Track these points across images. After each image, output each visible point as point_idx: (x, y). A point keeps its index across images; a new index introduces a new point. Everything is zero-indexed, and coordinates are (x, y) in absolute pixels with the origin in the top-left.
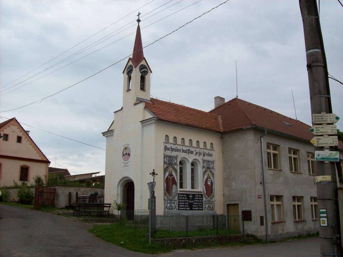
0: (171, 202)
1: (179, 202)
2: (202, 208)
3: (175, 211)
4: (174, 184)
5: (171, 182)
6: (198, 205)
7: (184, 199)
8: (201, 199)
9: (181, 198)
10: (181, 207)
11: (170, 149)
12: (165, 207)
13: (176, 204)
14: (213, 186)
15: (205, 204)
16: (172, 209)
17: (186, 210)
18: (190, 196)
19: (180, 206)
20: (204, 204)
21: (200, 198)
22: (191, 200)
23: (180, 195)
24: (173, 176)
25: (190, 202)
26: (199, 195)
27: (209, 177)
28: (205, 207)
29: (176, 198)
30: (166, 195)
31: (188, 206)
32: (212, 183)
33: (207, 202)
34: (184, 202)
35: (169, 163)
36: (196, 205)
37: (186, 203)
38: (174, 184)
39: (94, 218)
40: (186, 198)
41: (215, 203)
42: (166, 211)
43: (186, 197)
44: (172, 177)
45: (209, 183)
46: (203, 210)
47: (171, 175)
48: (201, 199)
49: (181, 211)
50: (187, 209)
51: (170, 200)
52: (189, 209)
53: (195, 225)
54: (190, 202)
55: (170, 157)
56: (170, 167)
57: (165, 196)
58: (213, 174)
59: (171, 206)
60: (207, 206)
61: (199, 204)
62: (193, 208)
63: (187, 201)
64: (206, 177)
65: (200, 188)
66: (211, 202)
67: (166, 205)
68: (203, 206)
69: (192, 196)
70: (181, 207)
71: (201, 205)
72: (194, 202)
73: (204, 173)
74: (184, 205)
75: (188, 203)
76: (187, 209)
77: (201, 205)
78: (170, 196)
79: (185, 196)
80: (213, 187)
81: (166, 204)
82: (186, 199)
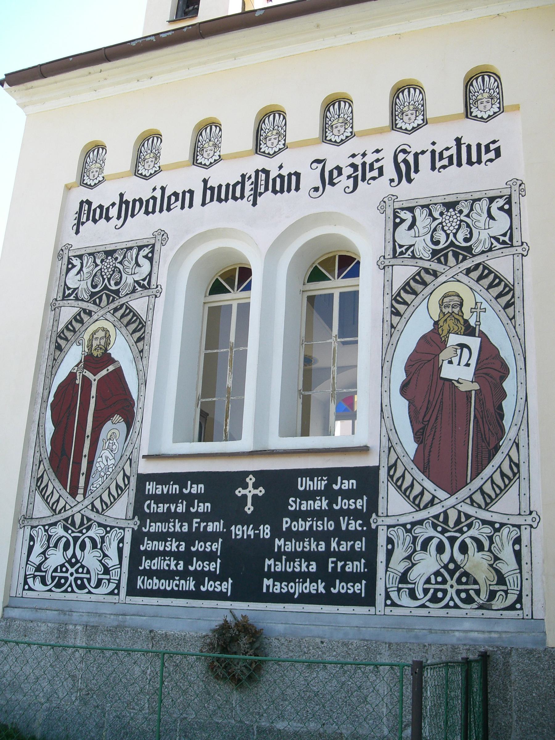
0: (76, 539)
1: (138, 538)
2: (359, 588)
3: (99, 602)
4: (117, 418)
5: (93, 402)
6: (321, 558)
7: (186, 517)
8: (361, 504)
9: (162, 508)
10: (150, 574)
11: (113, 212)
12: (31, 570)
13: (112, 552)
14: (509, 385)
15: (399, 553)
16: (82, 587)
17: (197, 595)
18: (240, 492)
19: (146, 564)
20: (389, 554)
21: (342, 504)
22: (245, 520)
23: (150, 487)
24: (111, 368)
25: (239, 531)
26: (331, 474)
27: (455, 319)
28: (404, 578)
29: (122, 509)
30: (42, 491)
31: (215, 566)
32: (492, 368)
33: (59, 531)
34: (179, 537)
35: (93, 295)
36: (292, 557)
37: (198, 546)
38: (117, 418)
39: (429, 693)
40: (204, 507)
41: (538, 543)
42: (30, 594)
43: (202, 498)
44: (104, 372)
45: (459, 371)
46: (380, 598)
47: (98, 360)
48: (361, 504)
49: (154, 601)
50: (208, 586)
51: (69, 524)
52: (226, 586)
53: (264, 723)
54: (239, 531)
55: (109, 253)
56: (95, 317)
57: (38, 498)
58: (506, 294)
59: (73, 562)
60: (427, 564)
61: (328, 553)
62: (267, 582)
63: (213, 527)
64: (419, 322)
65: (373, 423)
66: (95, 532)
67: (35, 559)
68: (372, 565)
69: (261, 491)
70: (150, 574)
71: (352, 556)
72: (277, 532)
73: (397, 299)
74: (177, 556)
75: (217, 547)
76: (208, 586)
77: (352, 556)
78: (73, 493)
79: (197, 489)
80: (503, 395)
81: (38, 549)
82: (197, 514)
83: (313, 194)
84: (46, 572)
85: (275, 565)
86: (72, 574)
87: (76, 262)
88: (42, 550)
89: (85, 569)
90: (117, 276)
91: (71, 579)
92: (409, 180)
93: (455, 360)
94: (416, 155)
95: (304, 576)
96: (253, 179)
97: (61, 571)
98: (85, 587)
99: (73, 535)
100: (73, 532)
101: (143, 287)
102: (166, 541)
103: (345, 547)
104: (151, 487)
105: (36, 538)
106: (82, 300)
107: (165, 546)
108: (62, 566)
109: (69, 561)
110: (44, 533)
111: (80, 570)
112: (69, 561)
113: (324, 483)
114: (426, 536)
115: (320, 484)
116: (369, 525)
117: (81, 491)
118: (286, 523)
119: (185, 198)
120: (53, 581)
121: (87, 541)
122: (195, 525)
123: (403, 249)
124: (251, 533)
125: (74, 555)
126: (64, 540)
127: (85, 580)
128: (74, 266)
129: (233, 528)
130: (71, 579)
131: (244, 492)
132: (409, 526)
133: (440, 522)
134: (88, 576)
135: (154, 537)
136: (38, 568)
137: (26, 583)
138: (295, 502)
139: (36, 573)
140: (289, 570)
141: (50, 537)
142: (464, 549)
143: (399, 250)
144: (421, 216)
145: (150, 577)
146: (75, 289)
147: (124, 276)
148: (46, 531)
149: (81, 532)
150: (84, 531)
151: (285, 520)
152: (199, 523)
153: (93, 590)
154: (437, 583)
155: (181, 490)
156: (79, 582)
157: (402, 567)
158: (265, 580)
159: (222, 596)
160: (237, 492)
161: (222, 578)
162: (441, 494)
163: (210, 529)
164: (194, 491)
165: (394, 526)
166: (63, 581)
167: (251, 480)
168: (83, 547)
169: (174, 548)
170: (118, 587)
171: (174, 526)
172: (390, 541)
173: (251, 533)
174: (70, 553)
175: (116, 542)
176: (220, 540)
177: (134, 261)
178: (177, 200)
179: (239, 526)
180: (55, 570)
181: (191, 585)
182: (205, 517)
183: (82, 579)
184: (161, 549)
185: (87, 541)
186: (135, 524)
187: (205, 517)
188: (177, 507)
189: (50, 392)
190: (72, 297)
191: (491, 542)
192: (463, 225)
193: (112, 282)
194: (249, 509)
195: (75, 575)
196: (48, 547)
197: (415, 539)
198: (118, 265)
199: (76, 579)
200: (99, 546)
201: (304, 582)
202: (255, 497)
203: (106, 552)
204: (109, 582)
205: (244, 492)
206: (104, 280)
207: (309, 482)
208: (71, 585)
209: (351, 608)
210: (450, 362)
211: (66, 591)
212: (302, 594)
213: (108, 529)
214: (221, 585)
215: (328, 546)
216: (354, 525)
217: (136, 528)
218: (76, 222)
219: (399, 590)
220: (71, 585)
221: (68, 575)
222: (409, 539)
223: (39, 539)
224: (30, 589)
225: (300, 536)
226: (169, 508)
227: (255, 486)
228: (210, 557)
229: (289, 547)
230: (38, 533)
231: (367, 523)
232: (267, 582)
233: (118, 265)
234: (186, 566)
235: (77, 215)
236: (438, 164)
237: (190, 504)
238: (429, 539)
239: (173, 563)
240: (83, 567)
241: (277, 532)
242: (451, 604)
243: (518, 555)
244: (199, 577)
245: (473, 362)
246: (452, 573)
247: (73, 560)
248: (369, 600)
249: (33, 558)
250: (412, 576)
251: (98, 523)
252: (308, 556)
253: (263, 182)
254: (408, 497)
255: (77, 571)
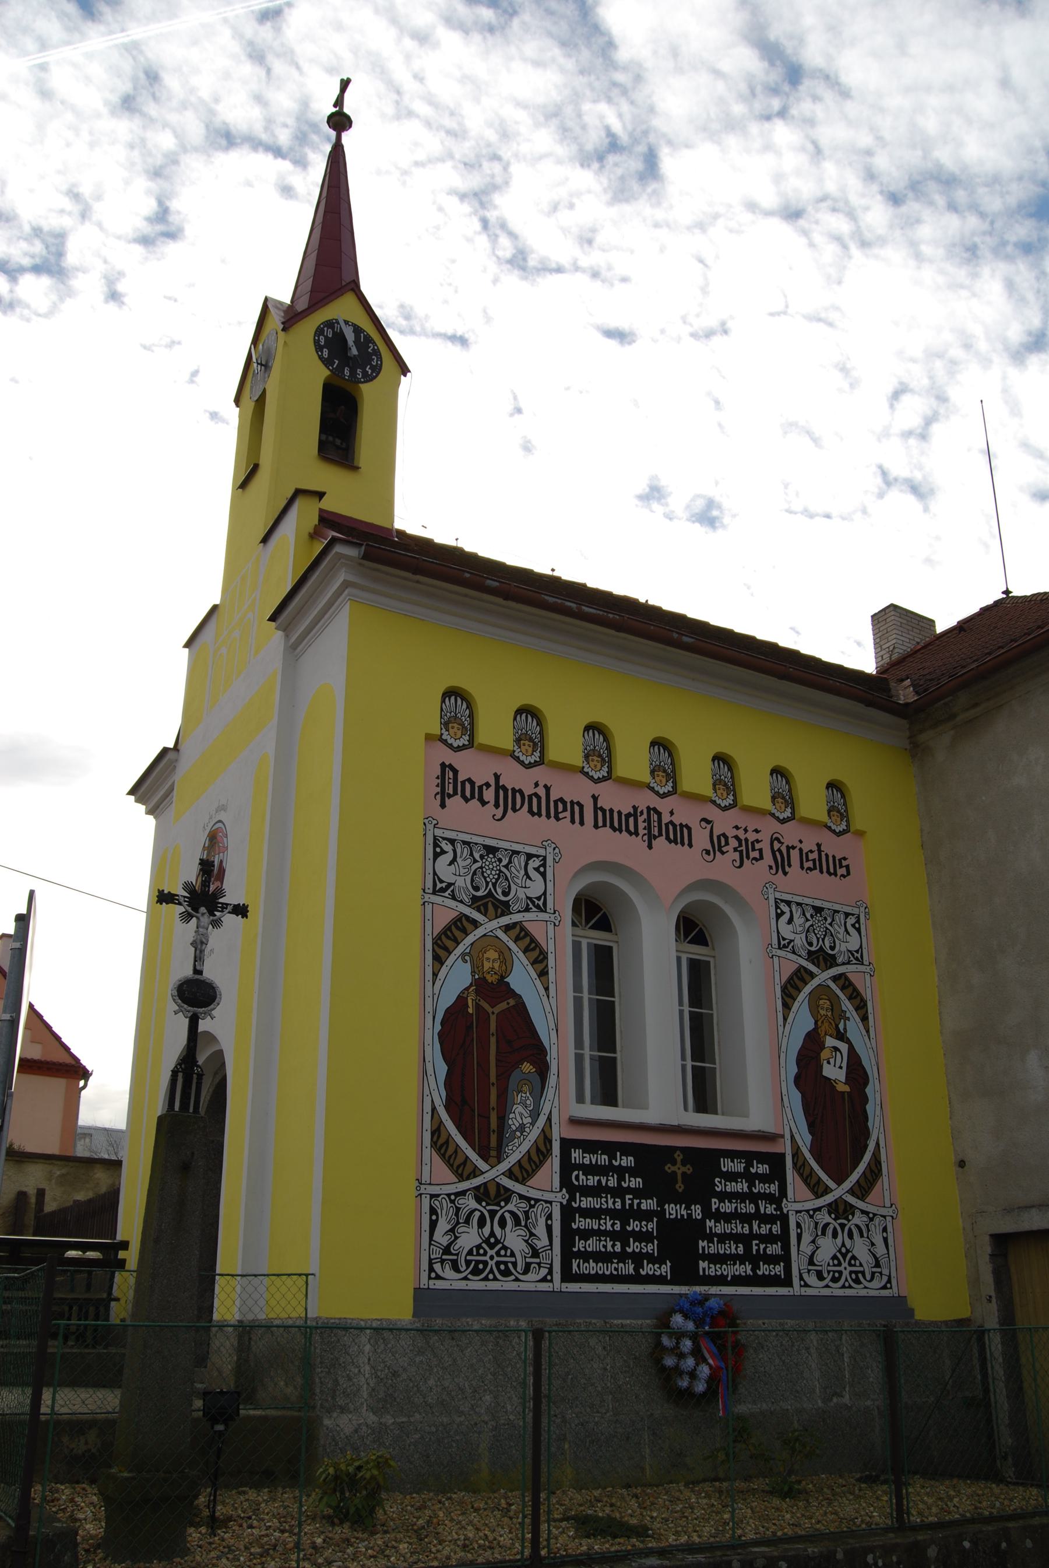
0: (493, 1214)
1: (568, 1213)
2: (779, 1269)
7: (618, 1192)
8: (774, 1188)
9: (592, 1181)
10: (586, 1256)
12: (437, 1253)
13: (541, 1230)
15: (806, 1238)
16: (506, 1273)
17: (637, 1279)
18: (669, 1168)
19: (580, 1245)
20: (799, 1237)
21: (759, 1188)
23: (576, 1155)
24: (512, 1002)
25: (673, 1211)
28: (811, 1262)
31: (652, 1248)
33: (824, 1218)
34: (613, 1214)
36: (723, 1238)
37: (634, 1226)
43: (633, 1172)
45: (834, 1071)
46: (796, 1280)
48: (774, 1188)
51: (481, 1194)
52: (666, 1269)
54: (673, 1211)
59: (491, 1241)
60: (827, 1248)
61: (752, 1236)
62: (703, 1265)
63: (648, 1204)
68: (786, 1247)
69: (688, 1169)
70: (586, 1256)
71: (770, 1238)
73: (437, 942)
74: (613, 1236)
75: (652, 1226)
76: (648, 1269)
77: (770, 1238)
79: (627, 1161)
81: (443, 1226)
82: (629, 1190)
83: (706, 856)
84: (457, 1255)
85: (709, 1247)
86: (492, 1258)
87: (447, 847)
88: (450, 1227)
89: (509, 1252)
90: (505, 884)
91: (492, 1263)
92: (785, 873)
93: (832, 1061)
94: (788, 848)
95: (734, 1258)
96: (645, 816)
97: (478, 1254)
98: (510, 1274)
99: (488, 1208)
100: (488, 1204)
101: (538, 907)
102: (600, 1219)
103: (764, 1230)
104: (577, 1155)
105: (439, 1211)
106: (461, 902)
107: (600, 1224)
108: (479, 1247)
109: (487, 1241)
110: (450, 1205)
111: (503, 1252)
112: (487, 1241)
113: (743, 1165)
114: (825, 1222)
115: (738, 1166)
116: (781, 1209)
117: (493, 1153)
118: (715, 1203)
119: (574, 810)
120: (468, 1267)
121: (507, 1215)
122: (628, 1202)
123: (444, 885)
124: (684, 1213)
125: (492, 1234)
126: (477, 1214)
127: (510, 1265)
128: (443, 852)
129: (666, 1206)
130: (492, 1263)
131: (673, 1168)
132: (811, 1213)
133: (481, 1194)
134: (513, 1259)
135: (586, 1213)
136: (447, 1250)
137: (431, 1269)
138: (720, 1182)
139: (444, 1257)
140: (722, 1252)
141: (458, 1209)
142: (503, 1224)
143: (782, 943)
144: (463, 852)
145: (586, 1261)
146: (450, 885)
147: (513, 887)
148: (811, 1217)
149: (498, 1204)
150: (503, 1204)
151: (713, 1200)
152: (632, 1200)
153: (521, 1277)
154: (834, 1265)
155: (610, 1161)
156: (502, 1267)
157: (445, 1241)
158: (701, 1262)
159: (660, 1280)
160: (666, 1168)
161: (660, 1261)
162: (482, 1165)
163: (643, 1207)
164: (624, 1163)
165: (800, 1212)
166: (481, 1266)
167: (678, 1156)
168: (503, 1224)
169: (609, 1228)
170: (550, 1272)
171: (607, 1202)
172: (798, 1225)
173: (684, 1213)
174: (487, 1231)
175: (544, 1219)
176: (655, 1219)
177: (522, 872)
178: (565, 810)
179: (672, 1205)
180: (470, 1252)
181: (629, 1268)
182: (637, 1193)
183: (505, 1263)
184: (596, 1227)
185: (507, 1215)
186: (562, 1197)
187: (637, 1193)
188: (608, 1180)
189: (434, 1018)
190: (446, 894)
191: (527, 1218)
192: (829, 934)
193: (499, 891)
194: (680, 1187)
195: (496, 1259)
196: (458, 1223)
197: (816, 1224)
198: (503, 869)
199: (498, 1264)
200: (523, 1223)
201: (735, 1264)
202: (684, 1174)
203: (533, 1231)
204: (540, 1267)
205: (673, 1168)
206: (487, 883)
207: (731, 1164)
208: (491, 1271)
209: (750, 1289)
210: (829, 1063)
211: (486, 1279)
212: (734, 1276)
213: (532, 1202)
214: (660, 1268)
215: (751, 1228)
216: (770, 1209)
217: (565, 1202)
218: (439, 789)
219: (809, 1271)
220: (491, 1271)
221: (487, 1258)
222: (812, 1225)
223: (444, 1212)
224: (438, 1277)
225: (728, 1218)
226: (599, 1181)
227: (684, 1164)
228: (643, 1237)
229: (719, 1228)
230: (441, 1203)
231: (779, 1208)
232: (703, 1265)
233: (503, 869)
234: (623, 1247)
235: (439, 781)
236: (806, 865)
237: (621, 1178)
238: (827, 1225)
239: (610, 1244)
240: (505, 1248)
241: (707, 1213)
242: (847, 1284)
243: (886, 1240)
244: (638, 1259)
245: (844, 1065)
246: (844, 1256)
247: (492, 1240)
248: (787, 1282)
249: (438, 1235)
250: (819, 1257)
251: (519, 1195)
252: (737, 1238)
253: (656, 824)
254: (452, 1166)
255: (498, 1254)
